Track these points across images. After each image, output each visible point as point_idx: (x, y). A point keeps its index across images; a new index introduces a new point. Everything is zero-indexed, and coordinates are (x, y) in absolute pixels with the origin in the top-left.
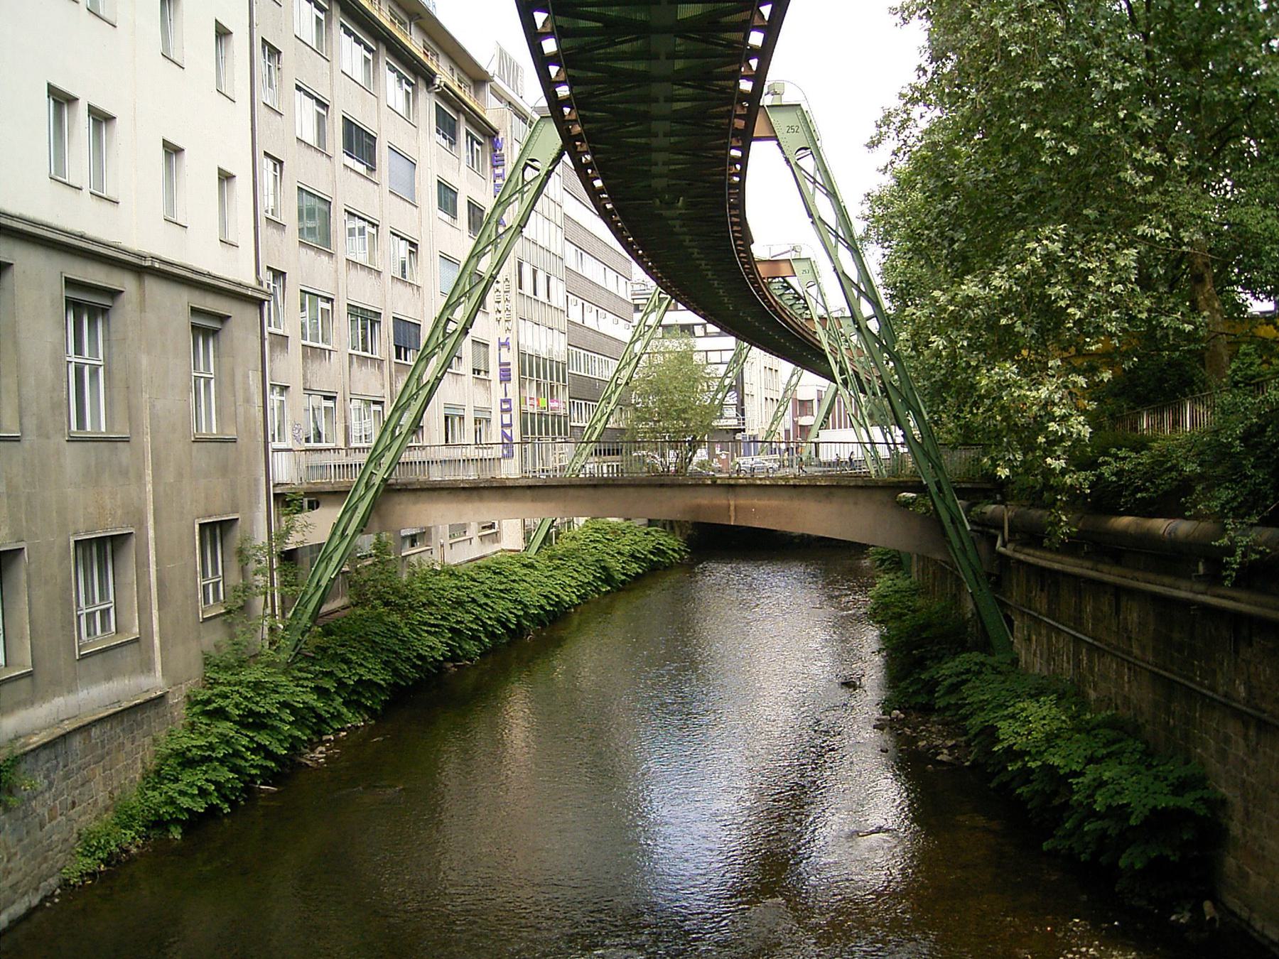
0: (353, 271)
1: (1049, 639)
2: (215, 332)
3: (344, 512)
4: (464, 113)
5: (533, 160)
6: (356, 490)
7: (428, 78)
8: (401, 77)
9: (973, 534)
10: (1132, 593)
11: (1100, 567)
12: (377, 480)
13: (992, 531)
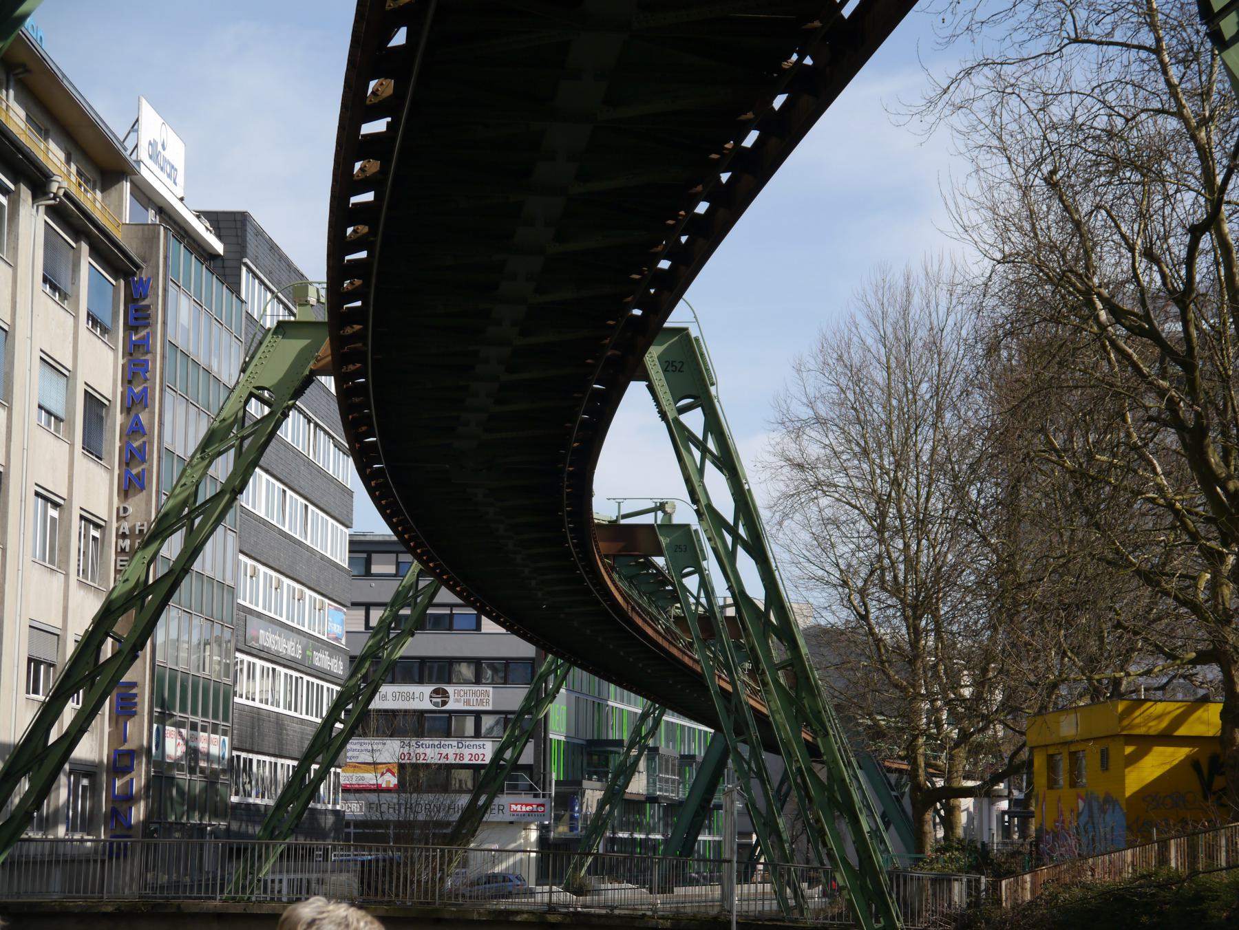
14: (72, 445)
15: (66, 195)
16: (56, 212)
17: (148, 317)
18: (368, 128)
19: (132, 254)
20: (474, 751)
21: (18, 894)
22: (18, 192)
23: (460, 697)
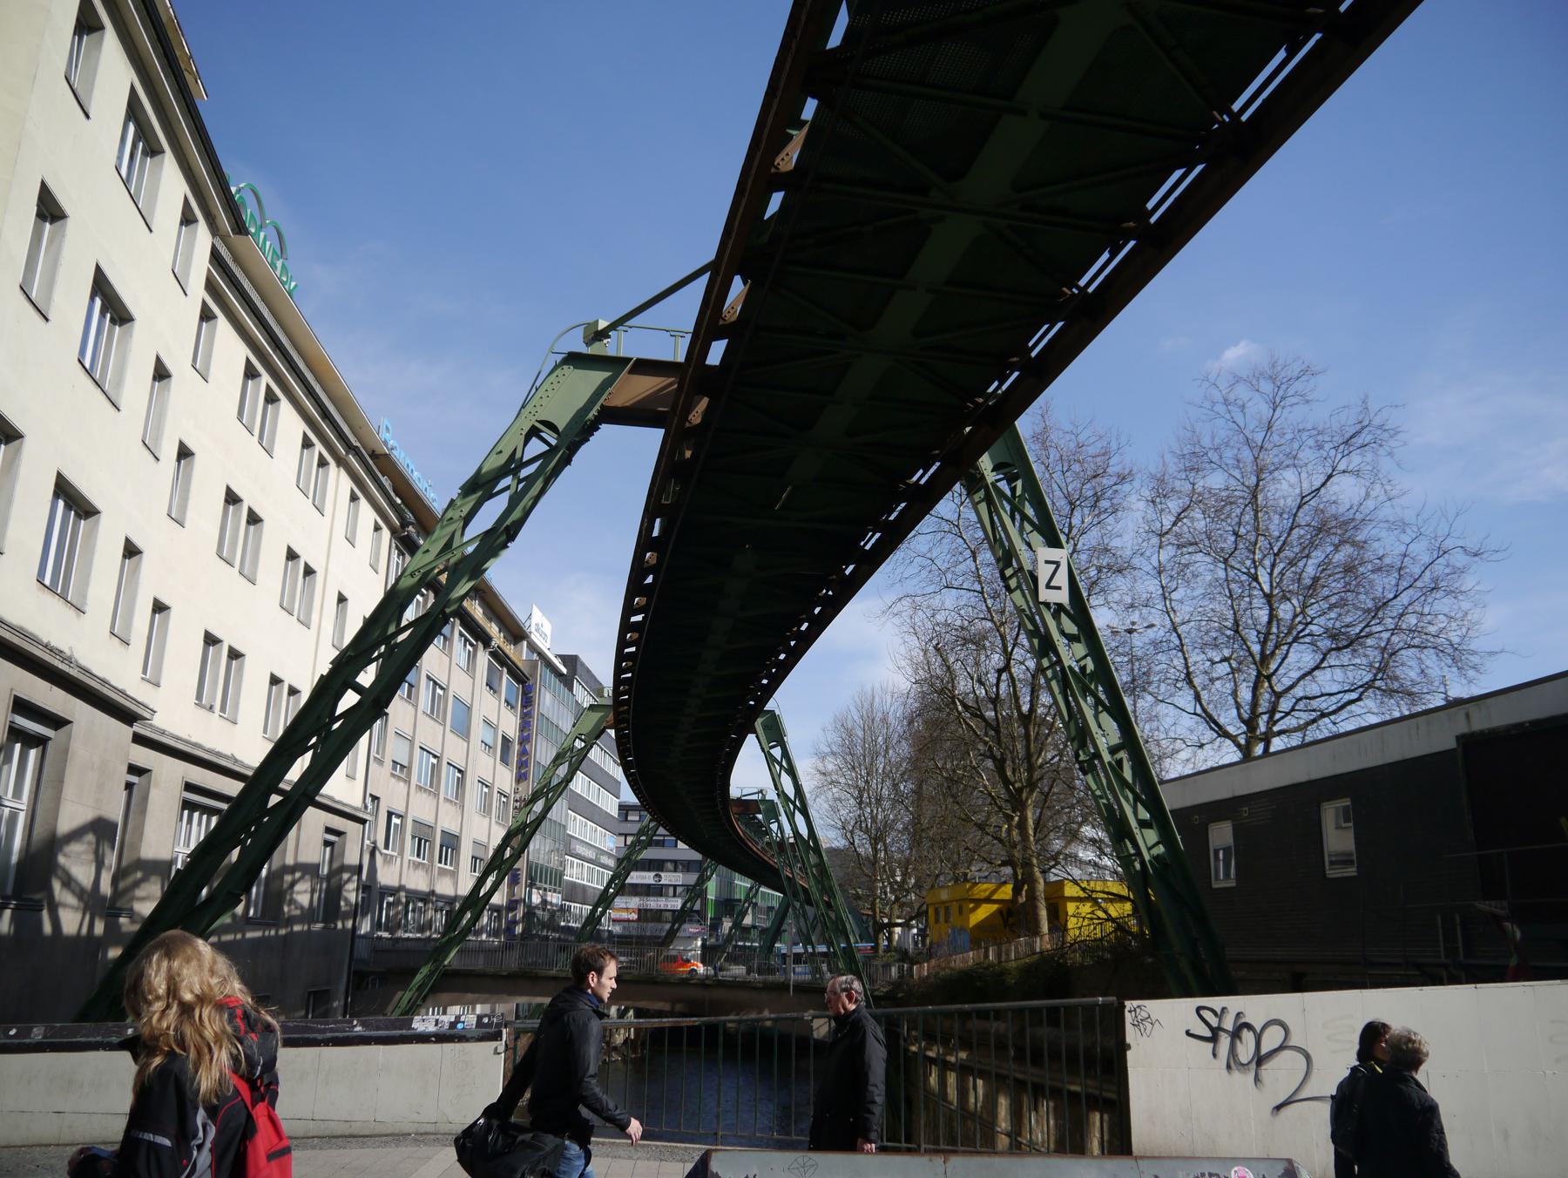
2: (41, 742)
7: (486, 640)
16: (493, 654)
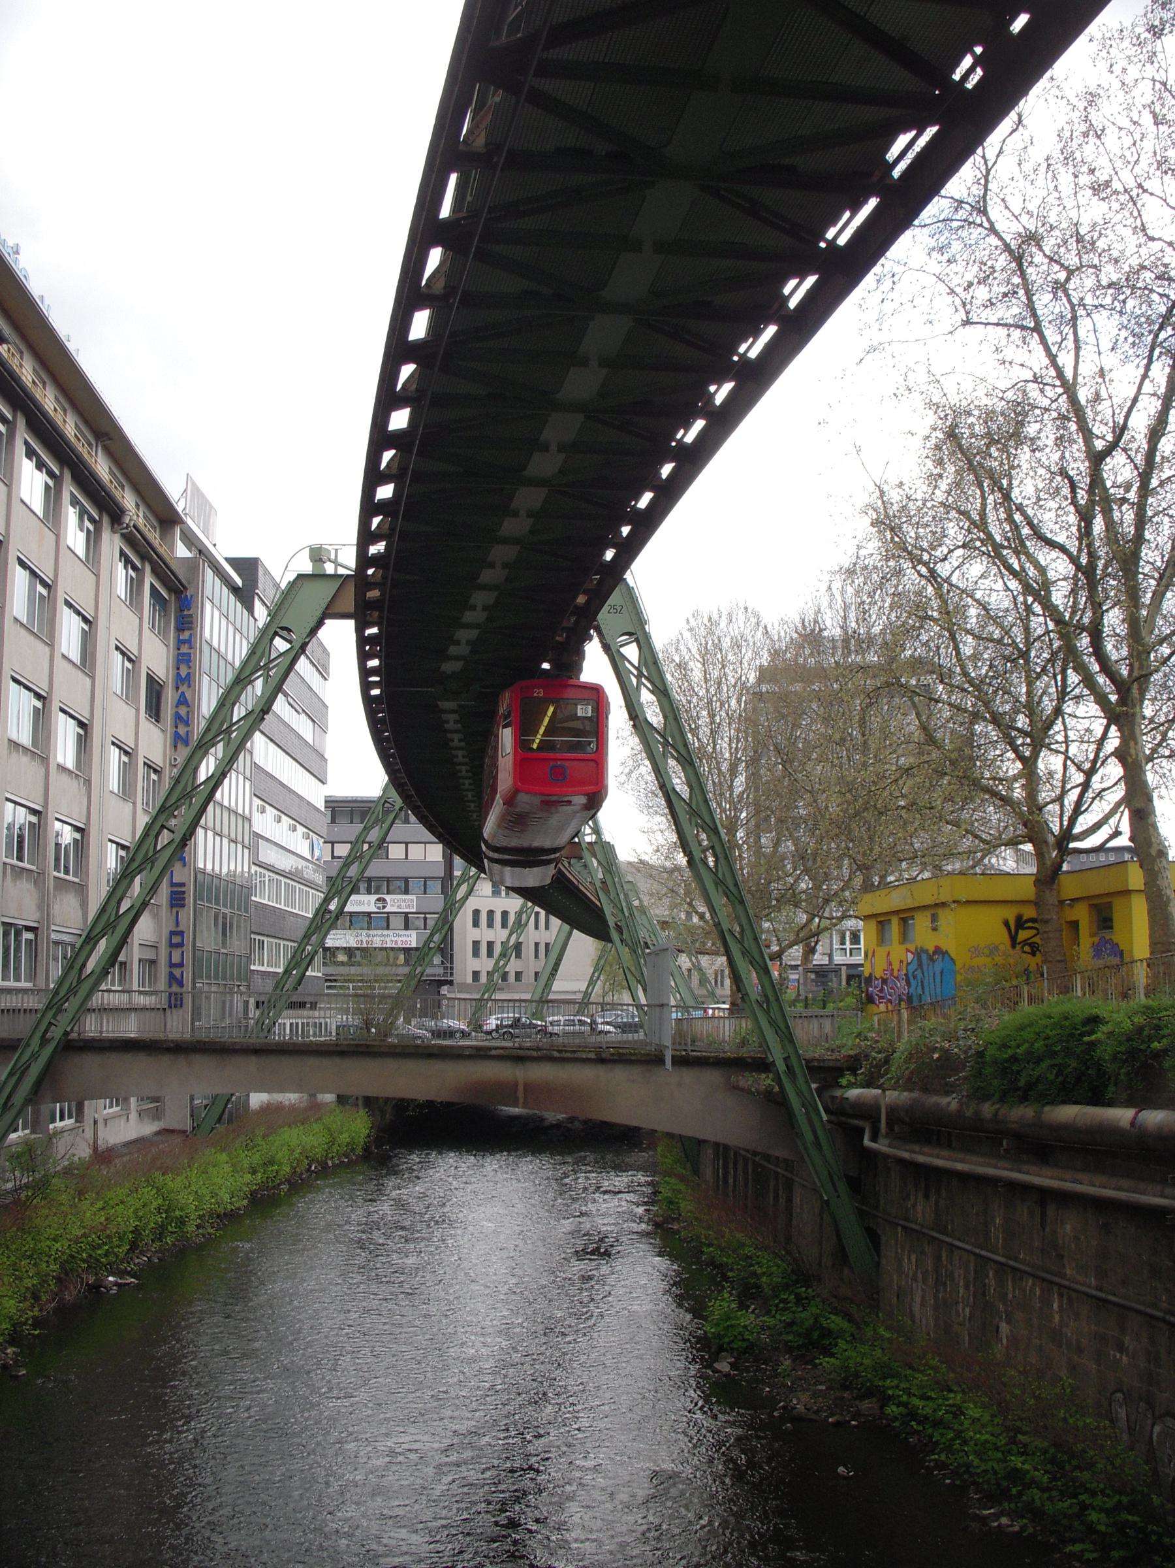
0: (14, 755)
1: (938, 1258)
3: (11, 1074)
4: (151, 562)
5: (288, 630)
6: (28, 1045)
7: (115, 514)
8: (83, 513)
9: (829, 1126)
10: (1063, 1198)
11: (1025, 1168)
12: (56, 1033)
13: (856, 1122)
14: (137, 710)
15: (134, 526)
16: (129, 539)
17: (192, 623)
18: (370, 594)
19: (183, 581)
20: (404, 939)
21: (108, 1031)
22: (143, 570)
23: (396, 903)
